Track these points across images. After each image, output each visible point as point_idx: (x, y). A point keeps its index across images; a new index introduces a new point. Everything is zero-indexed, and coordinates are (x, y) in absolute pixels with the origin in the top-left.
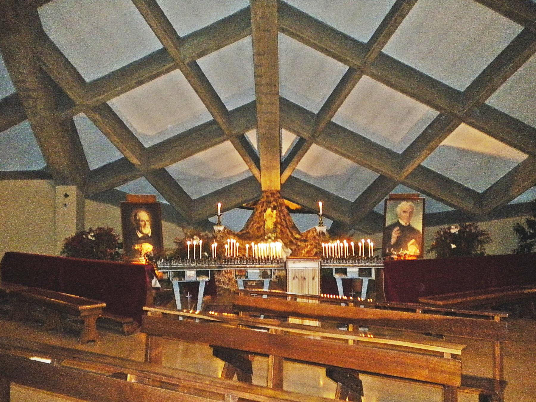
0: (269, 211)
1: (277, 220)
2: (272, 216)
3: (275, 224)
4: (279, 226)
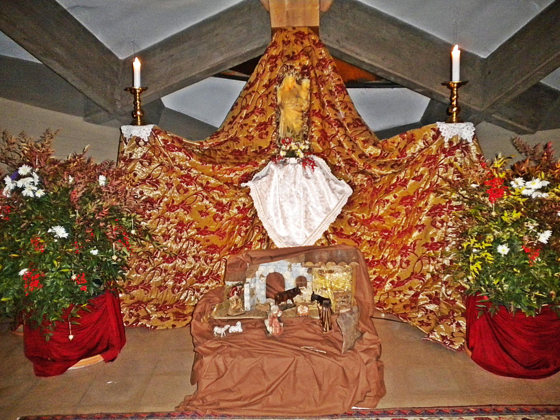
0: (290, 80)
1: (311, 105)
2: (298, 96)
3: (308, 115)
4: (317, 121)
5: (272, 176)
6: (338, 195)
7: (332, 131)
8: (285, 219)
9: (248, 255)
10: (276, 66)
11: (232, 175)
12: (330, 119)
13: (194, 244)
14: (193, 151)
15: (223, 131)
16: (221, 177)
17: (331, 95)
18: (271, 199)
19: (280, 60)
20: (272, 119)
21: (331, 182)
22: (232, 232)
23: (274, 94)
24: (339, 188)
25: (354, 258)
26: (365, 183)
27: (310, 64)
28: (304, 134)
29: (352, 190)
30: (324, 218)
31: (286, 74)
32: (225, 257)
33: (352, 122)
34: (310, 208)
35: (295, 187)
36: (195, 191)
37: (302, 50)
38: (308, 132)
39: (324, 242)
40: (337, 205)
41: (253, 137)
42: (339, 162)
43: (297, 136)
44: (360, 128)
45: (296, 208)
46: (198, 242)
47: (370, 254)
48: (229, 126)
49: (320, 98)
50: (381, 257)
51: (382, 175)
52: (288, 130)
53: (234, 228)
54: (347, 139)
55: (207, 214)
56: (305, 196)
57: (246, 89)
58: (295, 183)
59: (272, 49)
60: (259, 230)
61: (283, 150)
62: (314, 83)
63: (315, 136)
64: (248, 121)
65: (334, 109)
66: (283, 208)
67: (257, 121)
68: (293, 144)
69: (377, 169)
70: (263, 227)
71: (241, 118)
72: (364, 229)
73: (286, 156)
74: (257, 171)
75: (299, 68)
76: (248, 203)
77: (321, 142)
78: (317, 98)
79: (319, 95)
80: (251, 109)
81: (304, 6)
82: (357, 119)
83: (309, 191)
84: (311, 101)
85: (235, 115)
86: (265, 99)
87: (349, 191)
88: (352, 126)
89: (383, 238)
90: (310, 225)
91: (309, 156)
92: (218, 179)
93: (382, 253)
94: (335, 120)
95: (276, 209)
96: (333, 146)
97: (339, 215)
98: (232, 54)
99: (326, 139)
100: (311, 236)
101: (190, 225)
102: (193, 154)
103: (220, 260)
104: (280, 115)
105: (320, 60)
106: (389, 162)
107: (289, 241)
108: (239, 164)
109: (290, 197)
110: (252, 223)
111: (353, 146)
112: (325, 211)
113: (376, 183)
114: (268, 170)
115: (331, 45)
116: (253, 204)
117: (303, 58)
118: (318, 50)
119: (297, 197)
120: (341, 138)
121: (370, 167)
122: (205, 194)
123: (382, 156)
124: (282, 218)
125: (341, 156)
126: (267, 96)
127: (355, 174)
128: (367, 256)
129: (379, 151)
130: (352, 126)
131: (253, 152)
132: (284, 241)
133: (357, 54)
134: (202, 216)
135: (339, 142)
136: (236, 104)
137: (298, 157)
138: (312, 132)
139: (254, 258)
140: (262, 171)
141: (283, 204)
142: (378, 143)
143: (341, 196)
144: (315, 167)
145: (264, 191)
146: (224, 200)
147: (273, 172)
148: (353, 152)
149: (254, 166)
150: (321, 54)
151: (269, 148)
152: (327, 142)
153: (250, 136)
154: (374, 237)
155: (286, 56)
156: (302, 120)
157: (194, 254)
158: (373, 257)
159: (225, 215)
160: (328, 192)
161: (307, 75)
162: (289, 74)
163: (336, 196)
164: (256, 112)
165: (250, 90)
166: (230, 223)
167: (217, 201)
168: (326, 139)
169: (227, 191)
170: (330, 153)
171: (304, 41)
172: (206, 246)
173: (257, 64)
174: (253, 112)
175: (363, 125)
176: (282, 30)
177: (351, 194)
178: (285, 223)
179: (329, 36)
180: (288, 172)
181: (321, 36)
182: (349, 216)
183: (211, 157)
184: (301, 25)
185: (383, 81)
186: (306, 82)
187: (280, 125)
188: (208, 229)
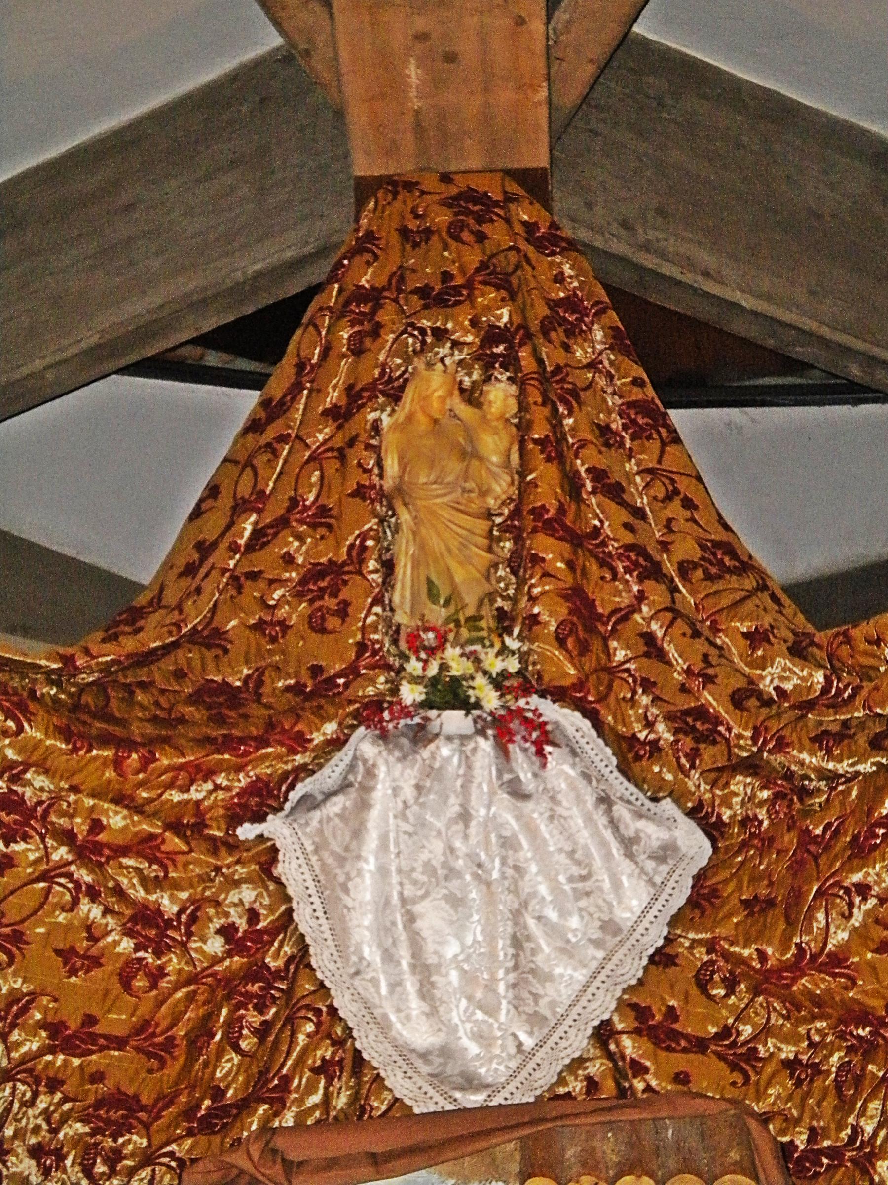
0: (433, 384)
1: (525, 488)
2: (469, 454)
4: (552, 552)
5: (366, 789)
6: (650, 865)
7: (618, 593)
8: (424, 971)
9: (275, 1152)
10: (376, 332)
11: (196, 794)
12: (604, 544)
13: (36, 1095)
14: (32, 692)
15: (157, 603)
16: (150, 801)
17: (607, 445)
18: (364, 890)
19: (390, 306)
20: (363, 548)
21: (620, 810)
22: (202, 1031)
23: (368, 447)
24: (653, 834)
25: (734, 1155)
26: (762, 814)
27: (517, 320)
28: (500, 609)
29: (707, 844)
30: (594, 965)
31: (419, 363)
32: (174, 1147)
33: (696, 554)
34: (531, 923)
35: (466, 837)
36: (44, 867)
37: (483, 265)
38: (514, 600)
39: (595, 1068)
40: (649, 907)
41: (284, 625)
42: (649, 725)
43: (468, 619)
44: (733, 581)
45: (475, 932)
46: (54, 1085)
47: (797, 1122)
48: (185, 582)
49: (560, 458)
50: (845, 1134)
51: (832, 777)
52: (432, 594)
53: (209, 1017)
54: (681, 626)
55: (95, 962)
56: (510, 872)
57: (254, 426)
58: (465, 816)
59: (359, 260)
60: (318, 1025)
61: (415, 680)
62: (535, 396)
63: (544, 617)
64: (263, 560)
65: (622, 503)
66: (419, 924)
67: (300, 560)
68: (452, 653)
69: (812, 753)
70: (333, 1011)
71: (234, 548)
72: (769, 1008)
73: (428, 704)
74: (305, 771)
75: (469, 338)
76: (271, 909)
77: (570, 643)
78: (549, 459)
79: (555, 448)
80: (275, 510)
81: (486, 90)
82: (717, 544)
83: (526, 851)
84: (522, 474)
85: (210, 535)
86: (332, 466)
87: (696, 847)
88: (699, 573)
89: (850, 1050)
90: (536, 997)
91: (522, 702)
92: (138, 809)
93: (851, 1120)
94: (628, 547)
95: (387, 930)
96: (620, 655)
97: (658, 951)
98: (189, 284)
99: (591, 629)
100: (540, 1045)
101: (17, 1016)
102: (32, 706)
103: (148, 1159)
104: (396, 530)
105: (559, 303)
106: (862, 724)
107: (449, 1070)
108: (228, 744)
109: (446, 878)
110: (288, 993)
111: (705, 657)
112: (597, 935)
113: (807, 813)
114: (352, 768)
115: (599, 243)
116: (290, 911)
117: (488, 296)
118: (545, 265)
119: (476, 877)
120: (654, 626)
121: (781, 745)
122: (87, 878)
123: (830, 699)
124: (413, 967)
125: (656, 700)
126: (342, 456)
127: (719, 775)
128: (783, 1132)
129: (819, 677)
130: (699, 573)
131: (288, 689)
132: (425, 1069)
133: (706, 274)
134: (73, 972)
135: (649, 638)
136: (213, 491)
137: (477, 705)
138: (533, 600)
139: (301, 1164)
140: (326, 770)
141: (418, 908)
142: (813, 644)
143: (664, 868)
144: (548, 749)
145: (333, 853)
146: (166, 901)
147: (370, 773)
148: (709, 680)
149: (293, 751)
150: (560, 279)
151: (352, 672)
152: (596, 645)
153: (272, 624)
154: (812, 1045)
155: (416, 291)
156: (490, 550)
157: (33, 1140)
158: (814, 1135)
159: (174, 963)
160: (608, 856)
161: (505, 367)
162: (430, 365)
163: (643, 871)
164: (294, 518)
165: (270, 434)
166: (190, 998)
167: (133, 903)
168: (591, 629)
169: (181, 859)
170: (610, 687)
171: (486, 228)
172: (91, 1099)
173: (297, 324)
174: (282, 523)
175: (746, 566)
176: (395, 185)
177: (704, 863)
178: (426, 992)
179: (589, 206)
180: (431, 772)
181: (556, 206)
182: (701, 954)
183: (110, 718)
184: (475, 163)
185: (814, 378)
186: (501, 394)
187: (399, 571)
188: (98, 1029)
